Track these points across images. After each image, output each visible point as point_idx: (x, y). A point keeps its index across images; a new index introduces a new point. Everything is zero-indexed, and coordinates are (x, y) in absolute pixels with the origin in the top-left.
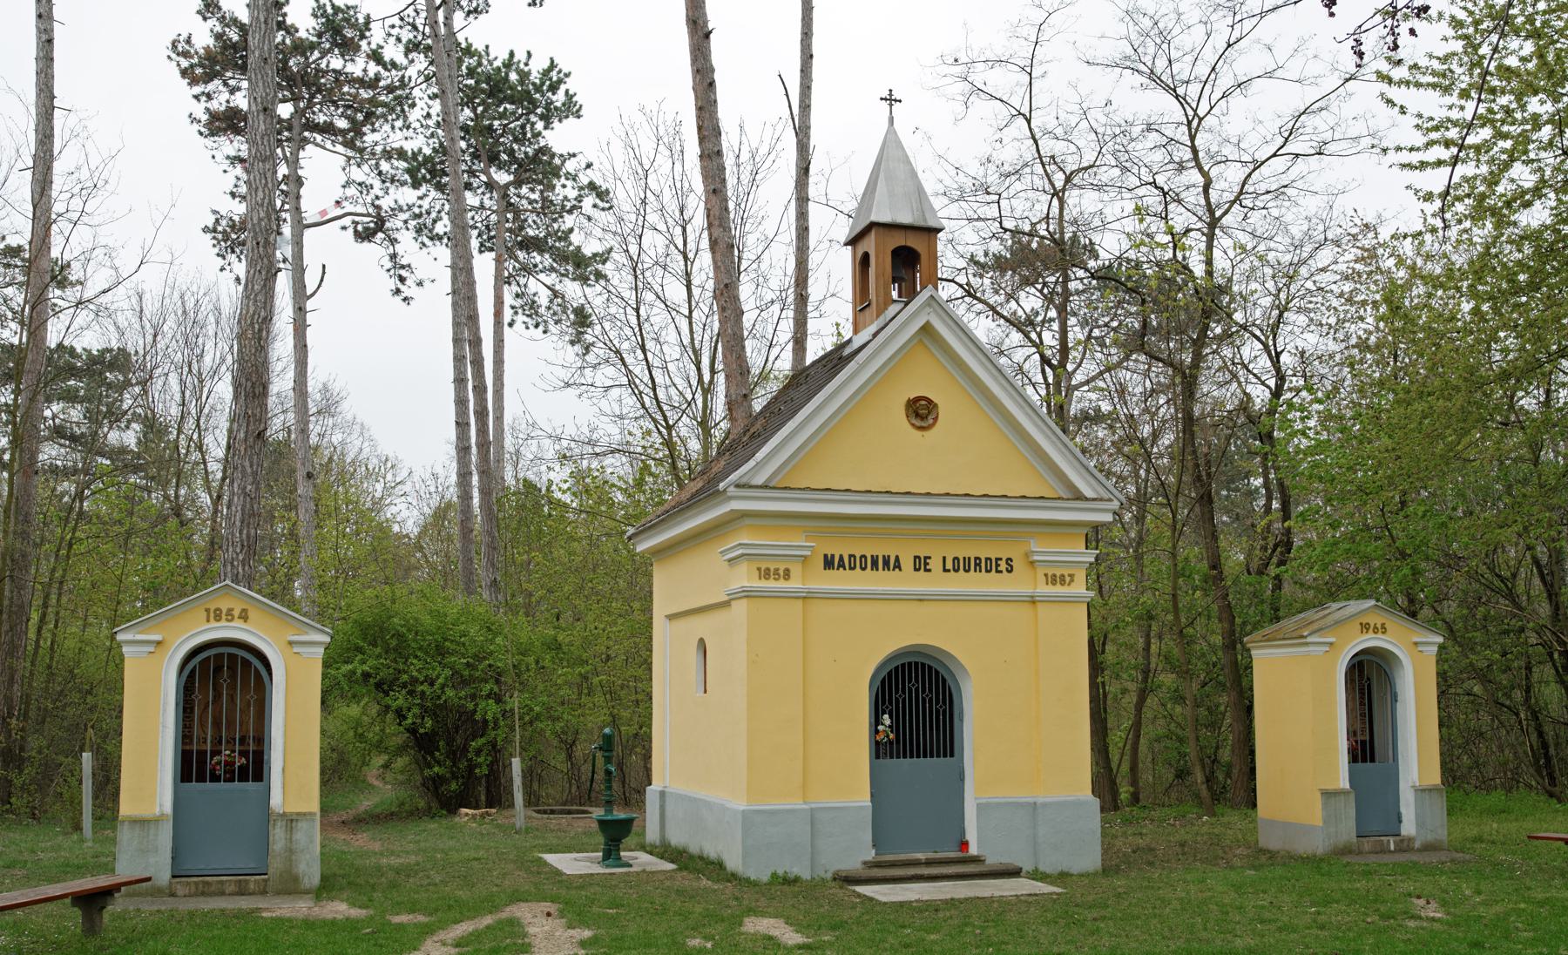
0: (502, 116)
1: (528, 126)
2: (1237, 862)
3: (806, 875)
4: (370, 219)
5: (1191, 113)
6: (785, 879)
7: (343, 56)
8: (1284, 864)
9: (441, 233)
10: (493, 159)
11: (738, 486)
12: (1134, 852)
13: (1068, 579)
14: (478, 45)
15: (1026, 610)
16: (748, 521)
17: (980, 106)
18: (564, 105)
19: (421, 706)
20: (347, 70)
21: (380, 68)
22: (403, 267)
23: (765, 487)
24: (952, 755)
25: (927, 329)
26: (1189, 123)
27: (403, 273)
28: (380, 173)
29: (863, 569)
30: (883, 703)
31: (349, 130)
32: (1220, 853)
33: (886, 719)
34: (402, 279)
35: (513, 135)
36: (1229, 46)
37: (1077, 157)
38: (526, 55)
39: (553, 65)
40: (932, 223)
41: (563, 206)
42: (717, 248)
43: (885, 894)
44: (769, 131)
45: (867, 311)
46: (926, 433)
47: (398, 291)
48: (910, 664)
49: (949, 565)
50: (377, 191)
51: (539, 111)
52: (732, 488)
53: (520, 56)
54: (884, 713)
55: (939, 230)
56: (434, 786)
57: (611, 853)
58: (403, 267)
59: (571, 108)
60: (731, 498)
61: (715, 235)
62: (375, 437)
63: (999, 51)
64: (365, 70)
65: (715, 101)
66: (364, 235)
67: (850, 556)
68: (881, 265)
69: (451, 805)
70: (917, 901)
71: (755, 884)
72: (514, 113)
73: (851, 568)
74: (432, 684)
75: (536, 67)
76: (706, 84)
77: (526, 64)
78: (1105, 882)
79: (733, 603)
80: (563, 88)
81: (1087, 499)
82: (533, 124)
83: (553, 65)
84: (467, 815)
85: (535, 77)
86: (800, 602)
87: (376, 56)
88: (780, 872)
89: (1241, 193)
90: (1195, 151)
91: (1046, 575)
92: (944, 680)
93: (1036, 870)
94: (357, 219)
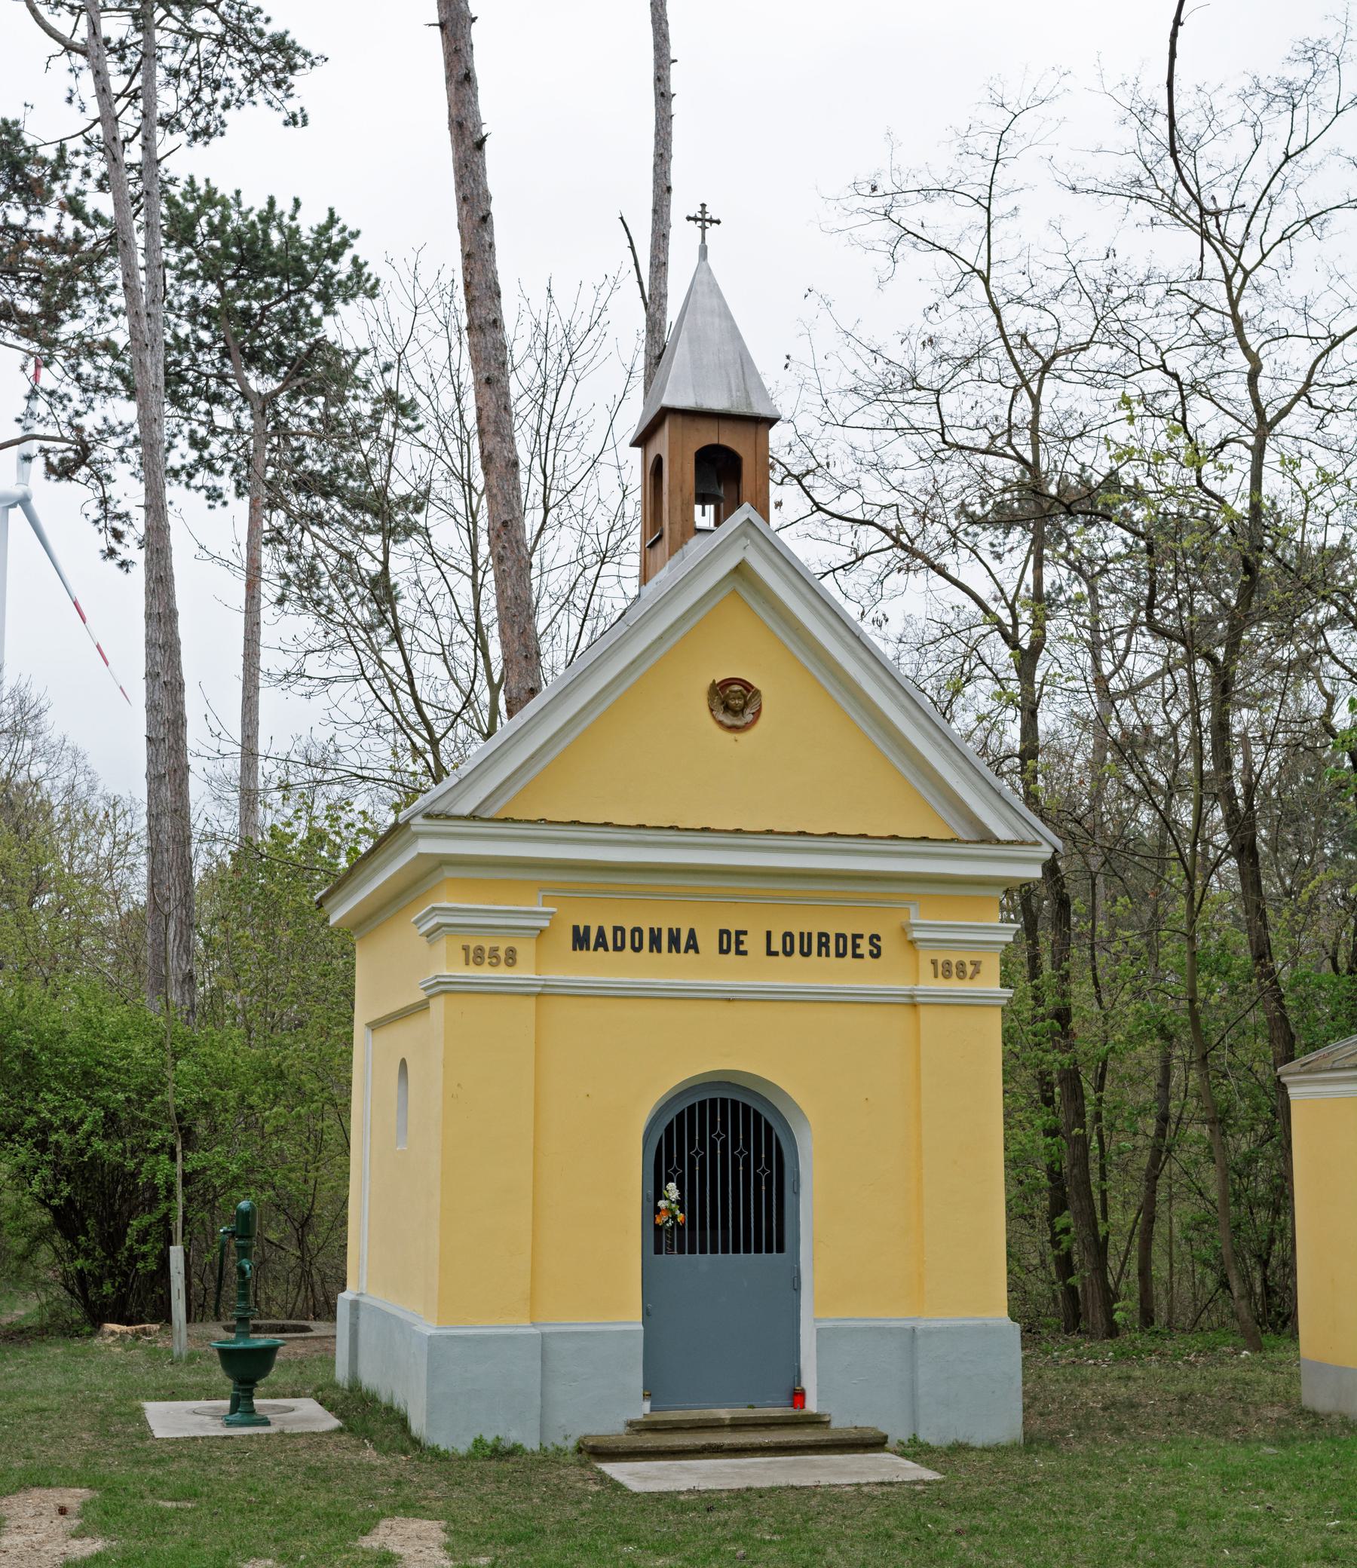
0: (259, 296)
1: (302, 311)
2: (1258, 1431)
3: (532, 1444)
4: (68, 445)
5: (1231, 263)
6: (495, 1450)
7: (26, 206)
8: (1332, 1438)
9: (177, 466)
10: (253, 358)
11: (428, 816)
12: (1105, 1409)
13: (970, 969)
14: (226, 190)
15: (902, 1018)
16: (448, 873)
17: (918, 262)
18: (349, 278)
19: (54, 1164)
20: (31, 227)
21: (79, 223)
22: (118, 517)
23: (472, 817)
24: (781, 1249)
25: (741, 570)
26: (1228, 280)
27: (118, 525)
28: (79, 378)
29: (637, 949)
30: (669, 1164)
31: (39, 316)
32: (1238, 1414)
33: (672, 1190)
34: (118, 535)
35: (280, 321)
36: (1288, 157)
37: (1053, 335)
38: (292, 203)
39: (332, 220)
40: (760, 409)
41: (355, 428)
42: (491, 467)
43: (646, 1479)
44: (588, 295)
45: (659, 547)
46: (743, 737)
47: (112, 553)
48: (713, 1101)
49: (777, 945)
50: (76, 405)
51: (314, 287)
52: (419, 820)
53: (284, 206)
54: (669, 1179)
55: (771, 422)
56: (81, 1284)
57: (242, 1406)
58: (118, 517)
59: (361, 284)
60: (417, 835)
61: (489, 447)
62: (93, 768)
63: (941, 175)
64: (59, 227)
65: (491, 245)
66: (63, 471)
67: (616, 929)
68: (681, 473)
69: (97, 1316)
70: (689, 1491)
71: (439, 1456)
72: (279, 290)
73: (616, 949)
74: (73, 1129)
75: (308, 222)
76: (476, 218)
77: (293, 218)
78: (1017, 1462)
79: (432, 1002)
80: (347, 256)
81: (999, 842)
82: (308, 307)
83: (332, 220)
84: (113, 1333)
85: (307, 236)
86: (531, 1002)
87: (73, 206)
88: (489, 1438)
89: (1308, 384)
90: (1238, 322)
91: (934, 962)
92: (769, 1129)
93: (914, 1440)
94: (47, 445)
